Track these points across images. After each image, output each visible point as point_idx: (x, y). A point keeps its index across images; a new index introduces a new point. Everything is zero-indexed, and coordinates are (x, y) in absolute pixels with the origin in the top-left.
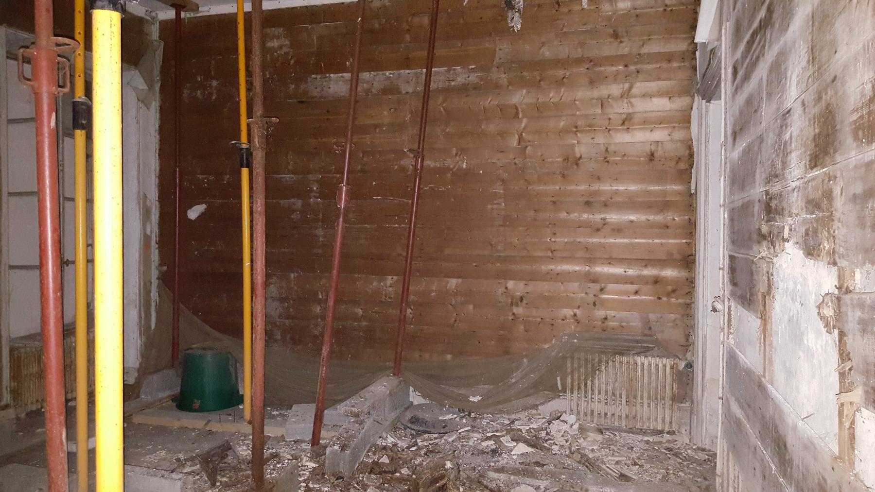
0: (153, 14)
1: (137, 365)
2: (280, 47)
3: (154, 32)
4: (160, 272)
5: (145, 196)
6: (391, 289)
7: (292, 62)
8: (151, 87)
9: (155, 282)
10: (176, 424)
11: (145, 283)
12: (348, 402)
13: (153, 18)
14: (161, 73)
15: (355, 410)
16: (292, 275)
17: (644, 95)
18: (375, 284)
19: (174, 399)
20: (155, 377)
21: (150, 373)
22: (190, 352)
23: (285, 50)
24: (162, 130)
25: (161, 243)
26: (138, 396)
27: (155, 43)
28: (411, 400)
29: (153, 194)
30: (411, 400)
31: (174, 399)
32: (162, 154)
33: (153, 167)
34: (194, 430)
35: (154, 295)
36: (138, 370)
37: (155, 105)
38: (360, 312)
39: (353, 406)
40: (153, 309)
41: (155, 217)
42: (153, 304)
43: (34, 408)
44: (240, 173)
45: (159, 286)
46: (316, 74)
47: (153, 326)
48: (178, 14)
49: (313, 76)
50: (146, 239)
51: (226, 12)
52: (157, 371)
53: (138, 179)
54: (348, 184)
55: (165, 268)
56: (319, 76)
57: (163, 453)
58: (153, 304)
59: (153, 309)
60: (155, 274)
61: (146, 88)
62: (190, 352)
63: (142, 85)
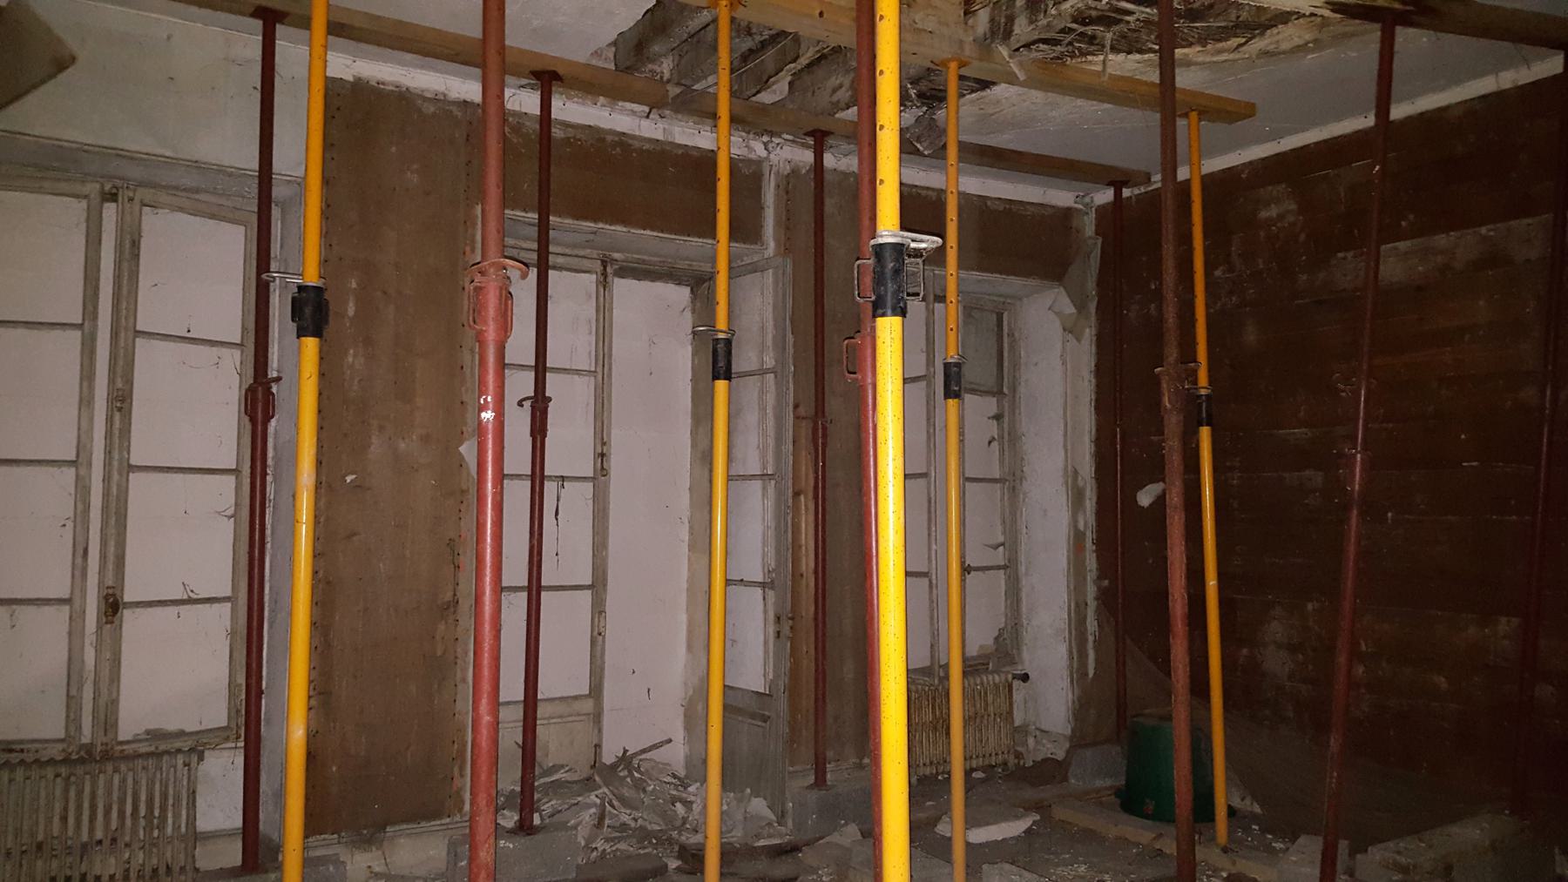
0: (1087, 200)
1: (1068, 732)
2: (1281, 217)
3: (1089, 226)
4: (1099, 588)
5: (1076, 472)
6: (1506, 642)
7: (1302, 237)
8: (1081, 308)
9: (1092, 605)
10: (1113, 832)
11: (1077, 605)
12: (1391, 844)
13: (1086, 205)
14: (1100, 283)
15: (1403, 860)
16: (1310, 606)
17: (602, 455)
18: (1472, 630)
19: (1118, 792)
20: (1089, 753)
21: (1086, 746)
22: (1141, 719)
23: (1291, 219)
24: (1099, 371)
25: (1098, 542)
26: (1065, 779)
27: (1090, 242)
28: (1558, 870)
29: (1087, 469)
30: (1558, 870)
31: (1118, 792)
32: (1100, 406)
33: (1087, 428)
34: (1137, 845)
35: (1092, 625)
36: (1071, 738)
37: (1089, 334)
38: (1442, 682)
39: (1399, 853)
40: (1090, 644)
41: (1090, 504)
42: (1091, 639)
43: (928, 771)
44: (1196, 433)
45: (1098, 612)
46: (1347, 250)
47: (1091, 673)
48: (1118, 194)
49: (1340, 255)
50: (1078, 538)
51: (1300, 144)
52: (1094, 744)
53: (1065, 446)
54: (1365, 449)
55: (1106, 583)
56: (1350, 255)
57: (1083, 868)
58: (1091, 639)
59: (1090, 644)
60: (1091, 591)
61: (1073, 310)
62: (1141, 719)
63: (1070, 309)
